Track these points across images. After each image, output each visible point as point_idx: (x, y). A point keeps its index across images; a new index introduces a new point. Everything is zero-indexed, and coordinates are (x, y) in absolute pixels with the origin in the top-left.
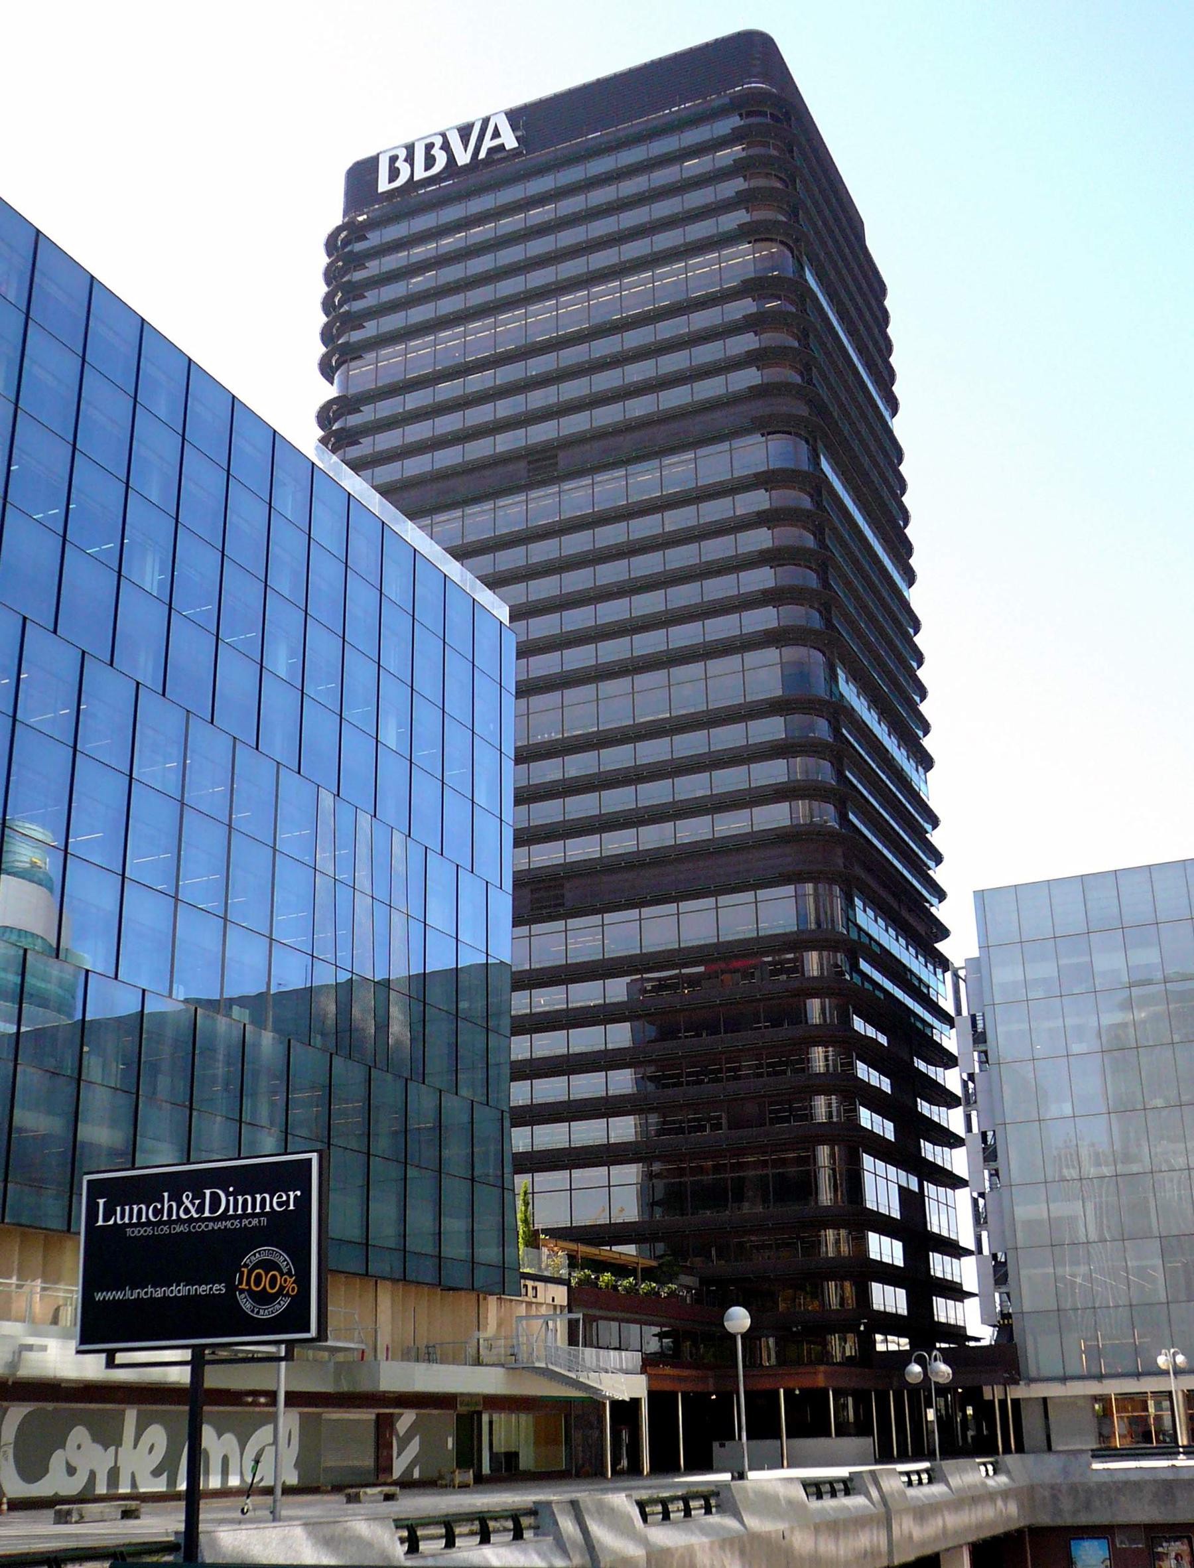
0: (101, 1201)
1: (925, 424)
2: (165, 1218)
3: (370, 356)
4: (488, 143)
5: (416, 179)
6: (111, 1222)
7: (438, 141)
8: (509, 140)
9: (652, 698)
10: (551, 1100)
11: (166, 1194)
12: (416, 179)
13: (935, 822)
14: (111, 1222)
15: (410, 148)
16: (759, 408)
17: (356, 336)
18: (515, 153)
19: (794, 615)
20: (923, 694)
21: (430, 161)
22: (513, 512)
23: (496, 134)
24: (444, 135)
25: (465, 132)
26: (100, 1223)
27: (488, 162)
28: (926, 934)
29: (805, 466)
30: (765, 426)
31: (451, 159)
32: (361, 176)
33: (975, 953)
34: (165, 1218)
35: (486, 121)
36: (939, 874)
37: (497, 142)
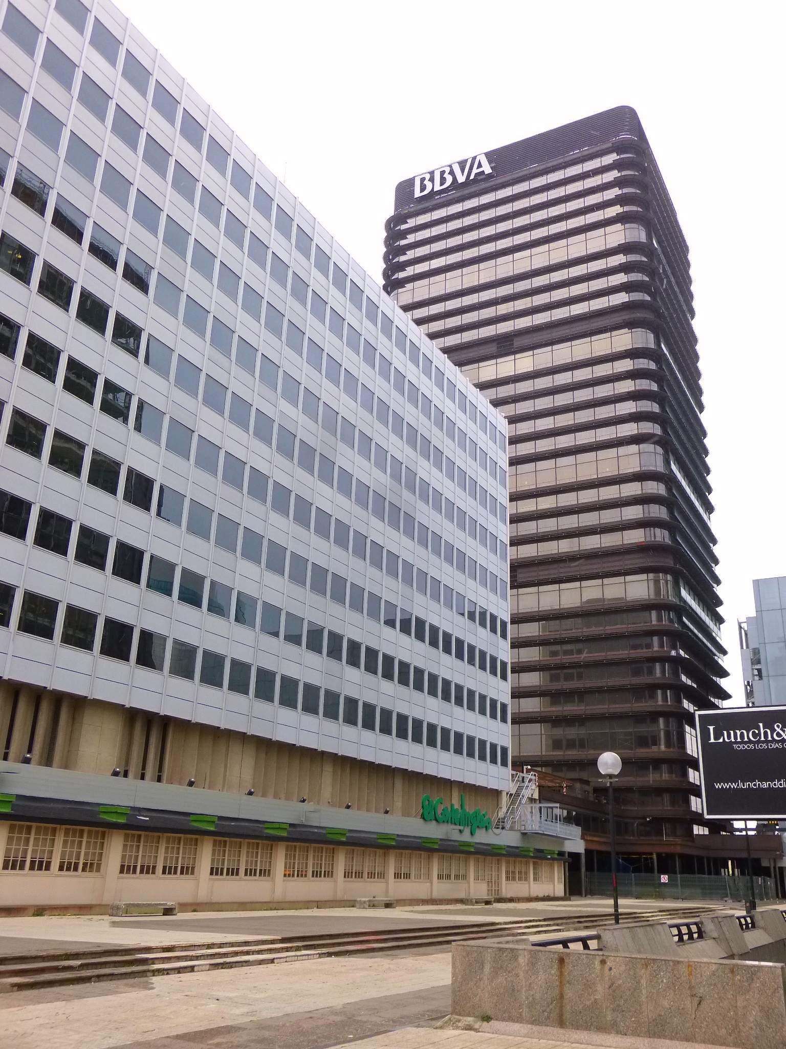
0: (711, 728)
1: (704, 324)
2: (763, 739)
3: (409, 286)
4: (475, 171)
5: (435, 190)
6: (721, 740)
7: (448, 170)
8: (487, 169)
11: (761, 725)
12: (435, 190)
13: (715, 542)
14: (721, 740)
16: (625, 316)
17: (402, 275)
18: (490, 176)
19: (647, 427)
20: (708, 472)
22: (506, 366)
24: (450, 166)
25: (462, 164)
26: (712, 740)
27: (475, 181)
28: (712, 602)
29: (652, 345)
30: (631, 325)
31: (455, 179)
32: (404, 190)
33: (753, 614)
34: (763, 739)
36: (716, 550)
37: (480, 170)
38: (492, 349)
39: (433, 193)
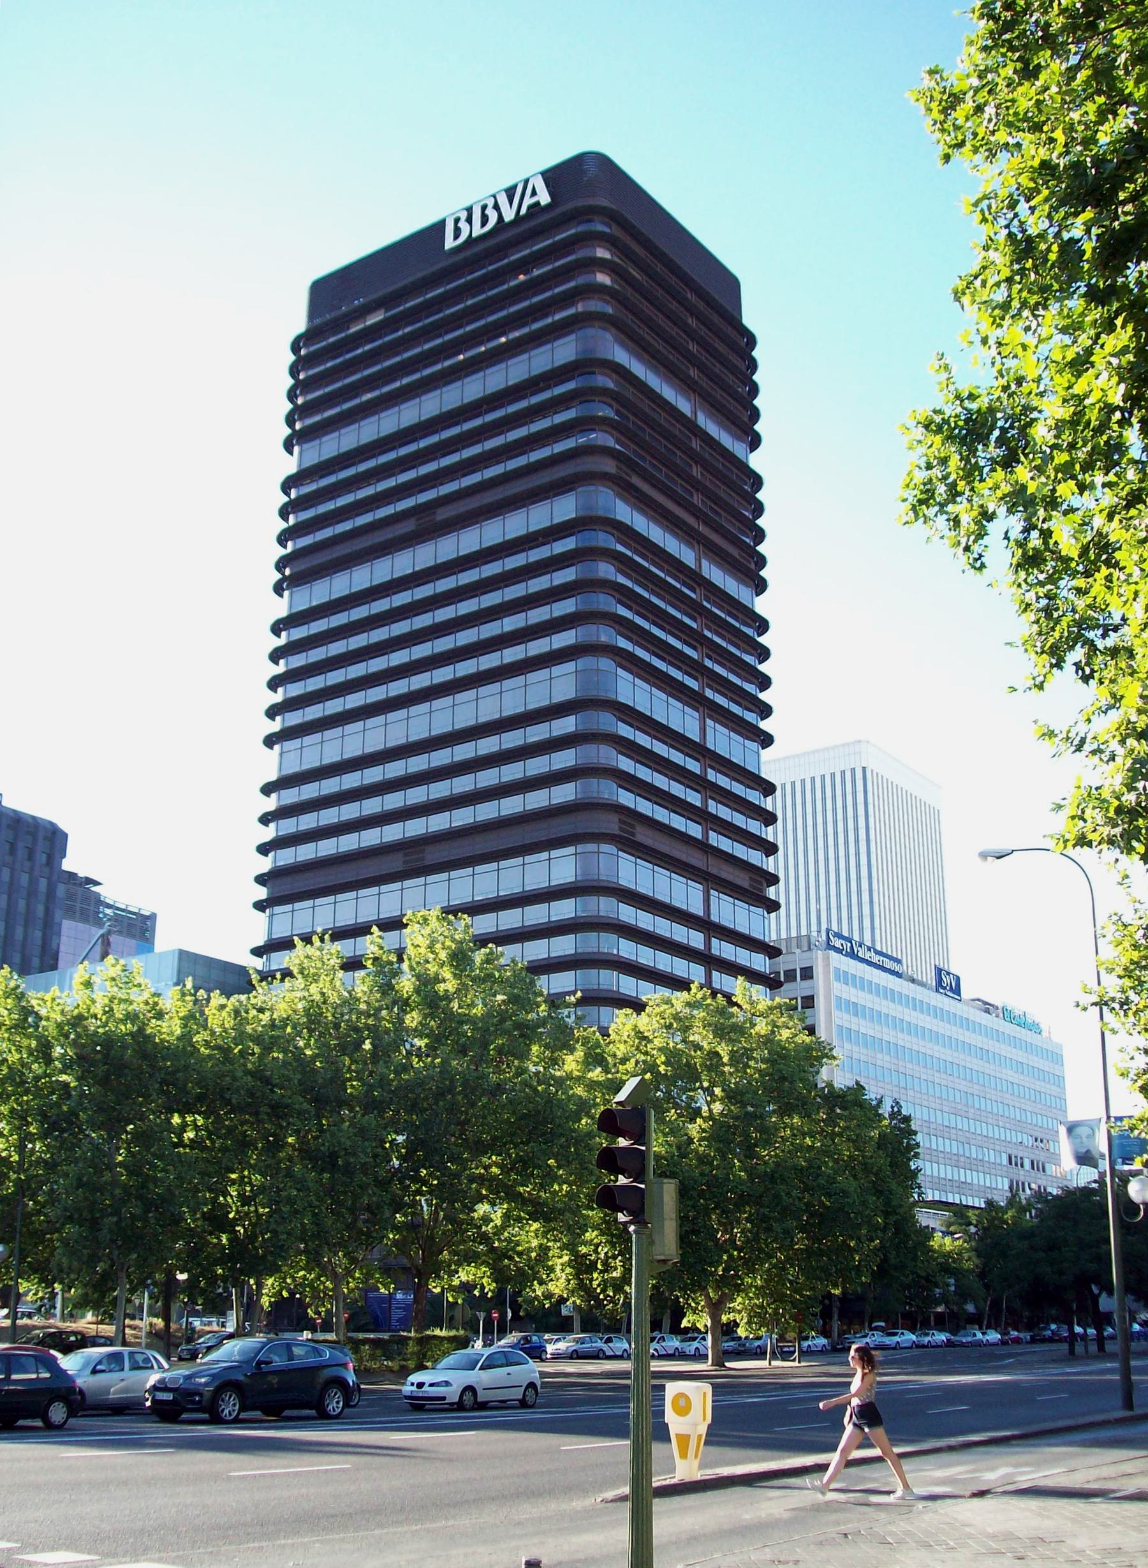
4: (528, 201)
5: (474, 235)
8: (544, 198)
9: (489, 703)
10: (551, 1435)
12: (474, 235)
15: (469, 210)
18: (549, 207)
21: (485, 220)
23: (534, 193)
25: (510, 192)
35: (526, 182)
38: (396, 863)
39: (470, 241)
